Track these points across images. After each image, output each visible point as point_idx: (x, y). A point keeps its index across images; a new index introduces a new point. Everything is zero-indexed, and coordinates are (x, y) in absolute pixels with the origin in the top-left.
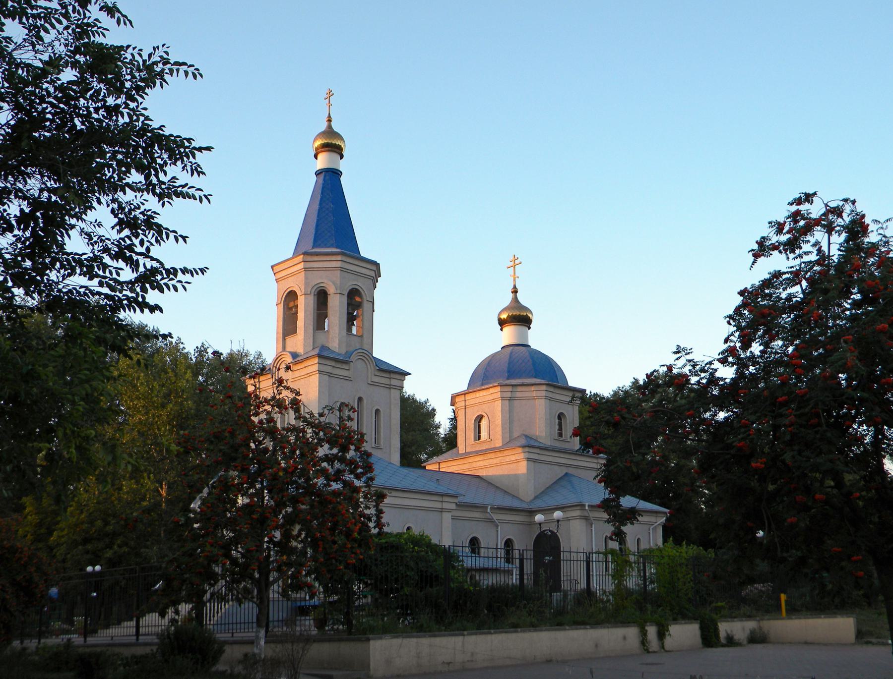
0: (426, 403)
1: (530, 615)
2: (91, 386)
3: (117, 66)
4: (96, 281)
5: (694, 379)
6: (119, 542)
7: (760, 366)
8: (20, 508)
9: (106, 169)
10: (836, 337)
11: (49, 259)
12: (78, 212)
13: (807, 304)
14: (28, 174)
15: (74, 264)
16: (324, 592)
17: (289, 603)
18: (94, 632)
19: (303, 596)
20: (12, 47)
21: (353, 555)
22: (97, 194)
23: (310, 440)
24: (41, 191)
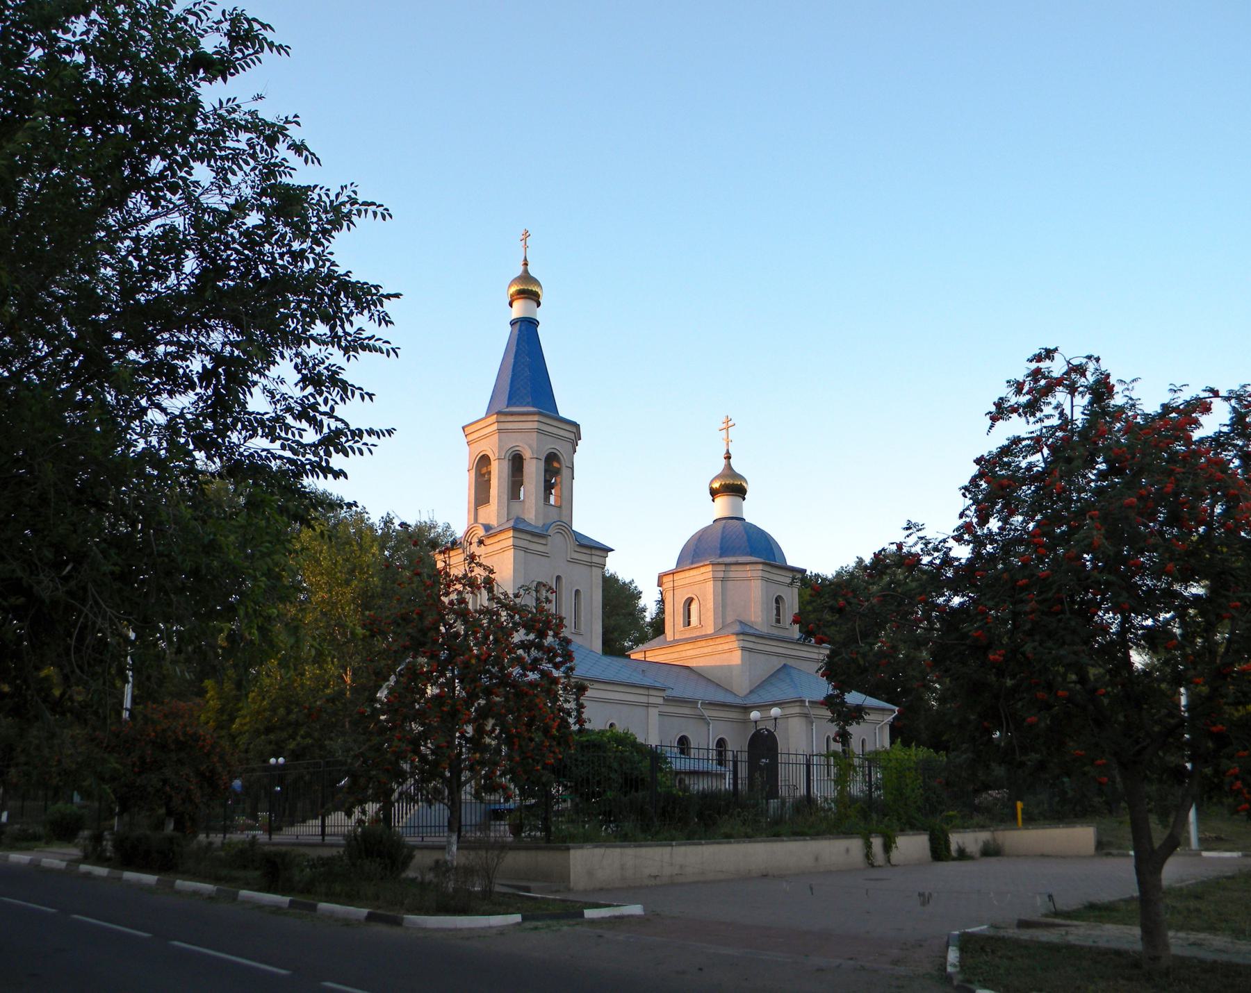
0: (631, 583)
1: (744, 824)
2: (273, 560)
3: (303, 208)
4: (278, 443)
5: (926, 560)
6: (302, 732)
7: (998, 544)
8: (202, 692)
9: (290, 320)
10: (1081, 513)
11: (231, 419)
12: (261, 368)
13: (1049, 474)
14: (211, 327)
15: (257, 425)
16: (520, 795)
17: (483, 806)
18: (280, 829)
19: (497, 798)
20: (199, 191)
21: (552, 755)
22: (280, 348)
23: (505, 623)
24: (224, 344)
